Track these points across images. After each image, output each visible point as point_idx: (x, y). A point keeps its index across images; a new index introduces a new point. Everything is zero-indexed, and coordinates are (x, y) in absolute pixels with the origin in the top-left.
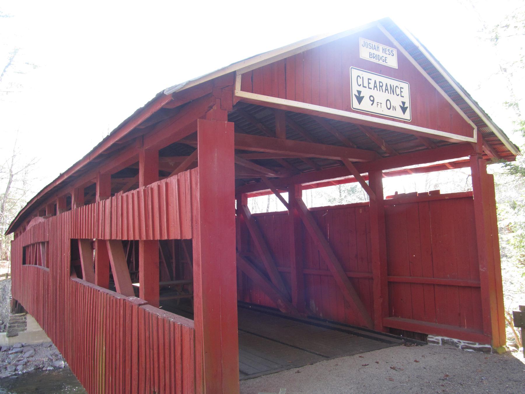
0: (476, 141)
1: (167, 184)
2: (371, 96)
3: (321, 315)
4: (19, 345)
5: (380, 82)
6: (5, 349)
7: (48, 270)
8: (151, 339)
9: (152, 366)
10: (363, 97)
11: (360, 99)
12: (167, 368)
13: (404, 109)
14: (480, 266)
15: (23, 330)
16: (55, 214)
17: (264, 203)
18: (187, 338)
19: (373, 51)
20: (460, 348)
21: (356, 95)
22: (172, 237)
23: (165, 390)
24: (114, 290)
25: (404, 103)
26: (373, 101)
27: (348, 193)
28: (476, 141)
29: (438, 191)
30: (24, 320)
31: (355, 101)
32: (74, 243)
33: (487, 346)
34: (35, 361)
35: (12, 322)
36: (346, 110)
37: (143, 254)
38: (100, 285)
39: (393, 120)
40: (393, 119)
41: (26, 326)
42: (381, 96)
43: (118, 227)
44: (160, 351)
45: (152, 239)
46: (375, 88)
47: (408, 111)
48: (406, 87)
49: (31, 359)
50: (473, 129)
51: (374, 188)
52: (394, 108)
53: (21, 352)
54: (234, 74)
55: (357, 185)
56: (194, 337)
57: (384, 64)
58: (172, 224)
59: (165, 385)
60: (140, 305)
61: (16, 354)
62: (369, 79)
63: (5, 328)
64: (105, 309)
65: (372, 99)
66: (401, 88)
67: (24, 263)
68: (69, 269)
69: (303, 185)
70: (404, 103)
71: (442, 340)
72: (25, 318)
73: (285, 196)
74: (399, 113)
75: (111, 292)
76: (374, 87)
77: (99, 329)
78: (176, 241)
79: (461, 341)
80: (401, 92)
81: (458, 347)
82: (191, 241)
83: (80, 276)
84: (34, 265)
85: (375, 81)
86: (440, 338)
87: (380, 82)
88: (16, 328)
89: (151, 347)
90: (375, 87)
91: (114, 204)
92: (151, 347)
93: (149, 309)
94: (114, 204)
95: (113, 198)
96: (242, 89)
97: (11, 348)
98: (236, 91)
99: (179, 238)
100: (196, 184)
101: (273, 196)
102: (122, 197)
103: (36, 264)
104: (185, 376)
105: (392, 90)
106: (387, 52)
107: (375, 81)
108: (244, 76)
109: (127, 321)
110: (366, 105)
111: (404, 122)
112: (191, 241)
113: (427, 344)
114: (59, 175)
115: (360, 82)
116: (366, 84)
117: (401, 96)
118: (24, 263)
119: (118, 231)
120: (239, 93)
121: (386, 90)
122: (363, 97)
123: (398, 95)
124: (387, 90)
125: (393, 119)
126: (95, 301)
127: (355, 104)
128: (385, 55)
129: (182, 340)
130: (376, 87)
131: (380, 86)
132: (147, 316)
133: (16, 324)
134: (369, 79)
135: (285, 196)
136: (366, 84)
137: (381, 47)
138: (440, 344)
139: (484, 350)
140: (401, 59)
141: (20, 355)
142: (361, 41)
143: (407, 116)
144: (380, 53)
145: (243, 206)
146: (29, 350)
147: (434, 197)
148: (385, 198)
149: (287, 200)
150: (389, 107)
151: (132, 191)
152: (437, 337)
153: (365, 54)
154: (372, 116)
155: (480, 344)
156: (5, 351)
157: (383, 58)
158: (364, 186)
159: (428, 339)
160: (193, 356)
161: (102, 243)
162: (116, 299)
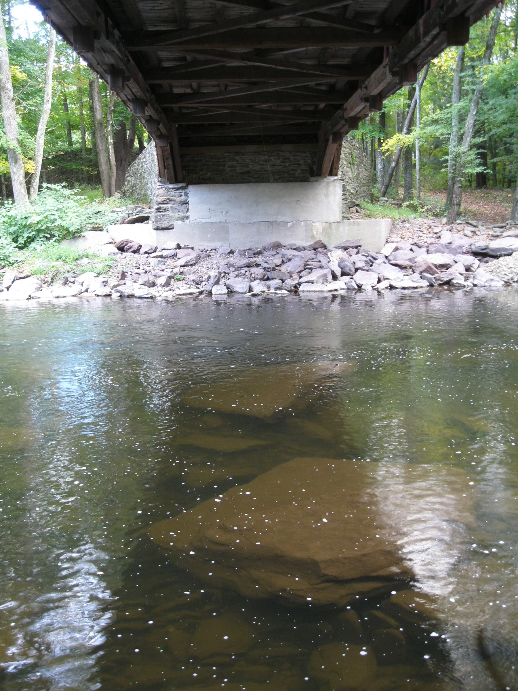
30: (183, 198)
35: (161, 199)
41: (188, 210)
49: (186, 269)
72: (186, 194)
133: (169, 206)
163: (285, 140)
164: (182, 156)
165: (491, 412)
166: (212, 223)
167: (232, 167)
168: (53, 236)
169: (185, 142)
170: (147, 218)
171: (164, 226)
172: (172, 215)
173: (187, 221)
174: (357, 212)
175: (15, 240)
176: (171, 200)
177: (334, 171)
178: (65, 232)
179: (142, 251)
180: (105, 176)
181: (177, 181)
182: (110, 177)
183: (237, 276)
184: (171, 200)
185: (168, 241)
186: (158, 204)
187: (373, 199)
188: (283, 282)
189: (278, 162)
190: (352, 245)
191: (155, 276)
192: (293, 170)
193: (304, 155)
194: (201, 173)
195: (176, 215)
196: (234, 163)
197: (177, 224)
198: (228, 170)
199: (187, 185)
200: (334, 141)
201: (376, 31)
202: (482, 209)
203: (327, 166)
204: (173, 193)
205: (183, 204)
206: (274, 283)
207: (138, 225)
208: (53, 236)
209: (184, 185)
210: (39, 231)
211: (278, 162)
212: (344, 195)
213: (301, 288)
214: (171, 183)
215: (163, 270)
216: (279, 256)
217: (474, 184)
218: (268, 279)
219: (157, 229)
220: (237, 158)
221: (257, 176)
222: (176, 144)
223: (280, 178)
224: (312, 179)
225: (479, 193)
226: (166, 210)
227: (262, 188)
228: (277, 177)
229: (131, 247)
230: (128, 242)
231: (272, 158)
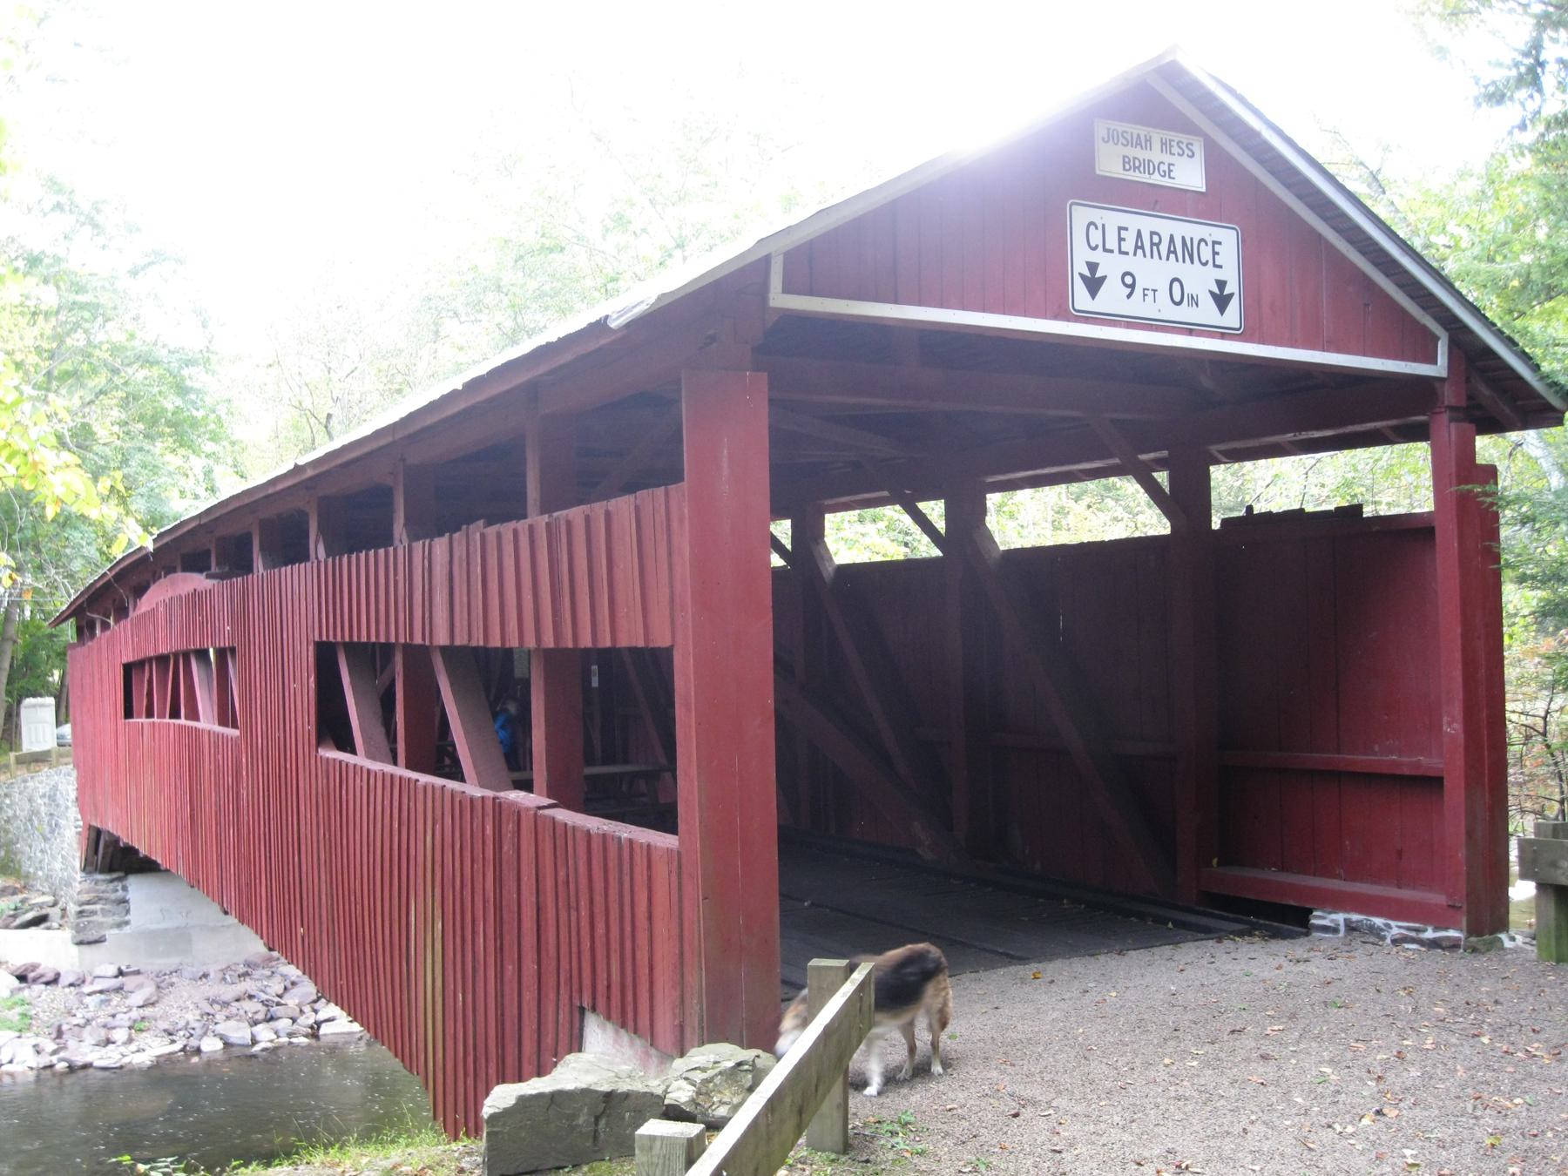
0: (1444, 374)
1: (608, 514)
2: (1126, 274)
3: (1038, 866)
4: (113, 970)
5: (1152, 233)
6: (71, 979)
7: (236, 733)
8: (572, 886)
9: (574, 949)
10: (1103, 278)
11: (1094, 284)
12: (615, 946)
13: (1222, 301)
14: (1445, 719)
15: (119, 925)
16: (248, 568)
17: (863, 537)
18: (661, 871)
19: (1132, 152)
20: (1388, 941)
21: (1082, 276)
22: (623, 643)
23: (608, 998)
24: (458, 775)
25: (1221, 284)
26: (1132, 286)
27: (1113, 511)
28: (1444, 374)
29: (1356, 509)
30: (120, 893)
31: (1080, 290)
32: (325, 656)
33: (1452, 933)
34: (165, 1016)
35: (85, 897)
36: (1056, 317)
37: (541, 683)
38: (410, 766)
39: (1190, 332)
40: (1189, 330)
41: (128, 912)
42: (1154, 272)
43: (473, 614)
44: (597, 911)
45: (570, 645)
46: (1140, 252)
47: (1234, 307)
48: (1228, 239)
49: (148, 1011)
50: (1436, 339)
51: (1187, 500)
52: (1194, 301)
53: (119, 989)
54: (767, 260)
55: (1130, 488)
56: (680, 867)
57: (1166, 182)
58: (622, 611)
59: (609, 987)
60: (540, 808)
61: (103, 997)
62: (1120, 229)
63: (63, 917)
64: (438, 827)
65: (1128, 280)
66: (1214, 243)
67: (129, 714)
68: (313, 728)
69: (990, 480)
70: (1221, 284)
71: (1348, 923)
72: (125, 889)
73: (935, 510)
74: (1207, 313)
75: (452, 785)
76: (1137, 247)
77: (420, 881)
78: (633, 651)
79: (1393, 923)
80: (1215, 253)
81: (1383, 938)
82: (669, 651)
83: (346, 744)
84: (167, 720)
85: (1139, 233)
86: (1340, 917)
87: (1152, 233)
88: (99, 918)
89: (573, 904)
90: (1139, 246)
91: (460, 552)
92: (573, 904)
93: (563, 815)
94: (460, 552)
95: (456, 535)
96: (787, 289)
97: (89, 979)
98: (771, 295)
99: (641, 644)
100: (681, 521)
101: (894, 513)
102: (483, 536)
103: (175, 714)
104: (658, 957)
105: (1189, 252)
106: (1175, 150)
107: (1139, 233)
108: (790, 257)
109: (505, 848)
110: (1111, 298)
111: (1223, 336)
112: (669, 651)
113: (1307, 934)
114: (291, 467)
115: (1096, 238)
116: (1112, 243)
117: (1215, 266)
118: (129, 714)
119: (474, 624)
120: (779, 299)
121: (1169, 252)
122: (1103, 278)
123: (1205, 264)
124: (1175, 252)
125: (1189, 330)
126: (405, 807)
127: (1081, 298)
128: (1167, 159)
129: (650, 878)
130: (1142, 248)
131: (1152, 244)
132: (559, 832)
133: (98, 907)
134: (1120, 229)
135: (935, 510)
136: (1112, 243)
137: (1157, 136)
138: (1341, 934)
139: (1444, 944)
140: (1217, 163)
141: (116, 999)
142: (1101, 130)
143: (1233, 317)
144: (1156, 155)
145: (809, 536)
146: (140, 986)
147: (1347, 521)
148: (1216, 524)
149: (941, 525)
150: (1177, 299)
151: (513, 524)
152: (1333, 916)
153: (1110, 164)
154: (1129, 326)
155: (1436, 929)
156: (71, 985)
157: (1164, 167)
158: (1152, 489)
159: (1313, 921)
160: (676, 908)
161: (418, 657)
162: (472, 800)
165: (506, 710)
166: (166, 930)
171: (91, 938)
172: (102, 918)
173: (127, 929)
176: (100, 899)
179: (64, 980)
181: (111, 870)
183: (228, 1018)
184: (100, 899)
185: (103, 964)
186: (81, 905)
188: (294, 1020)
190: (68, 678)
191: (105, 1026)
195: (110, 920)
197: (111, 934)
204: (103, 887)
206: (284, 1024)
207: (33, 930)
213: (322, 1031)
214: (102, 872)
215: (114, 1016)
216: (277, 978)
218: (272, 1019)
219: (80, 943)
226: (94, 913)
229: (42, 976)
230: (34, 967)
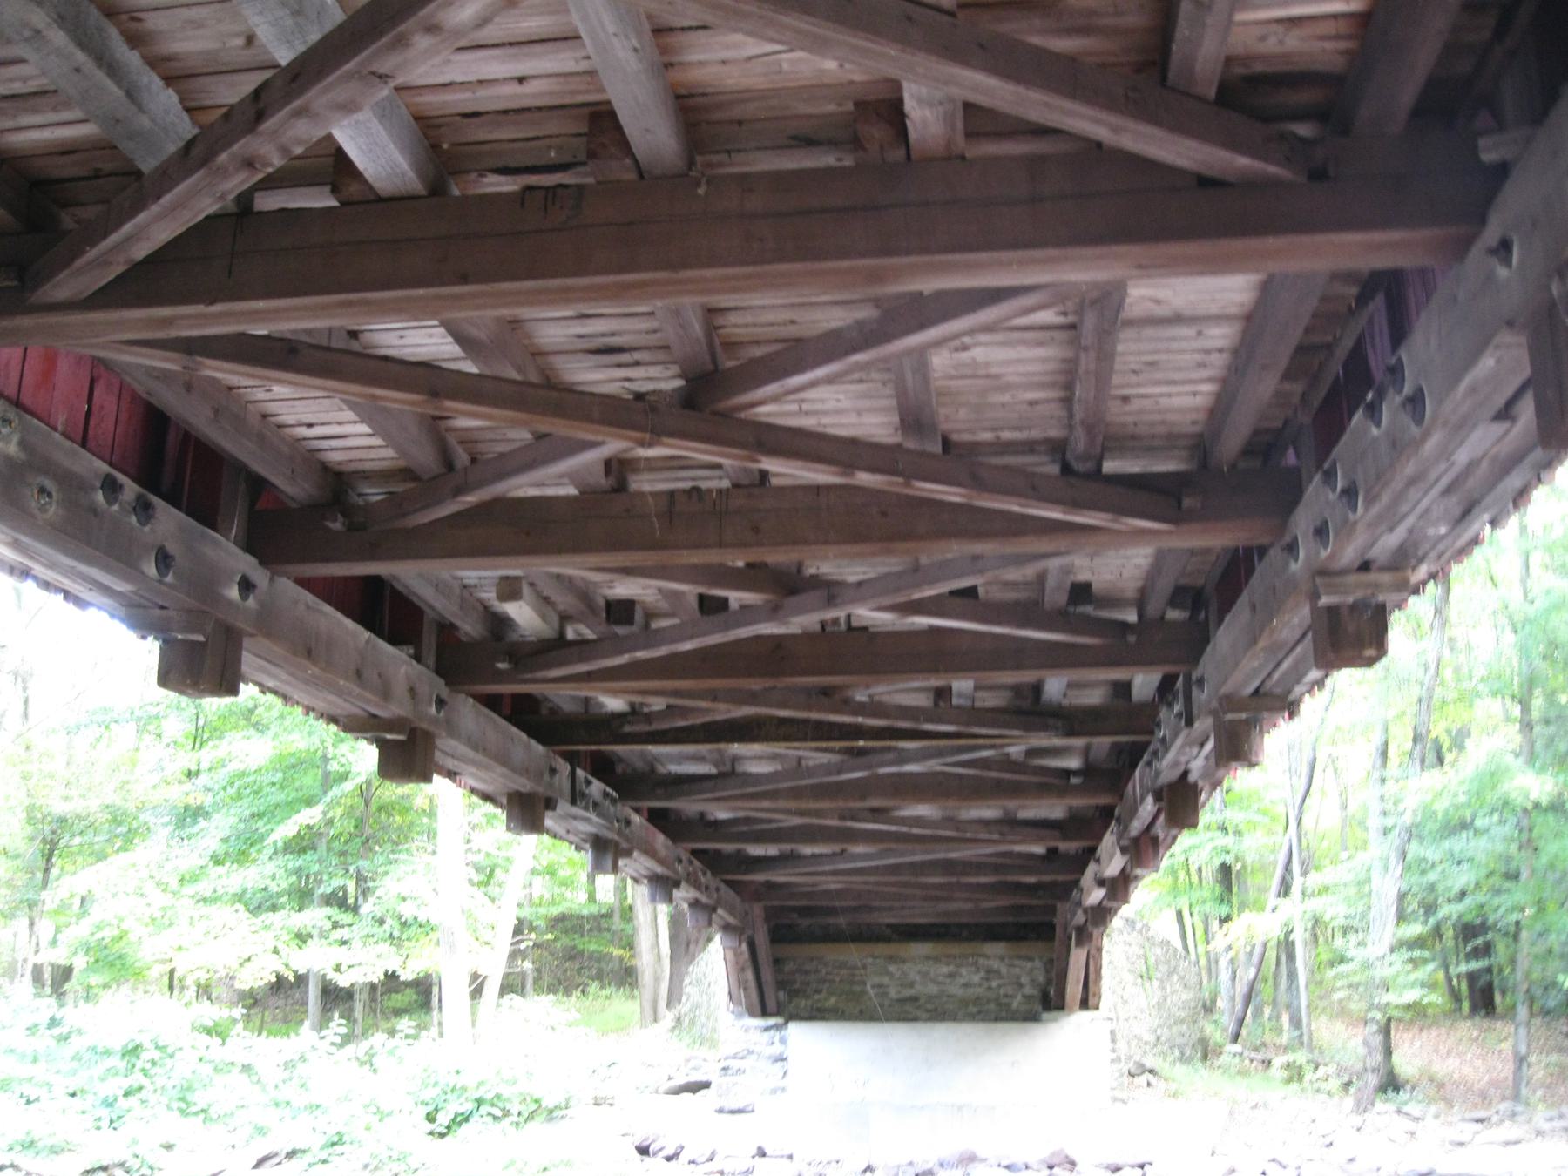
30: (777, 1049)
72: (783, 1041)
163: (992, 933)
164: (777, 962)
167: (880, 986)
168: (506, 1113)
169: (782, 933)
170: (707, 1085)
174: (1149, 1084)
175: (431, 1118)
176: (751, 1052)
177: (1091, 1001)
178: (534, 1107)
180: (646, 977)
182: (657, 980)
184: (751, 1052)
187: (1206, 1052)
189: (976, 979)
192: (1006, 996)
193: (1029, 965)
194: (816, 997)
196: (886, 980)
198: (872, 992)
199: (786, 1022)
200: (1079, 943)
201: (1074, 780)
202: (1466, 1070)
203: (1074, 990)
205: (776, 1061)
208: (506, 1113)
209: (780, 1020)
210: (480, 1102)
211: (976, 979)
212: (1114, 1051)
214: (752, 1014)
217: (1466, 1005)
220: (892, 968)
221: (929, 1006)
222: (762, 939)
223: (979, 1012)
224: (1045, 1015)
225: (1468, 1028)
227: (941, 1033)
228: (975, 1010)
231: (963, 971)
